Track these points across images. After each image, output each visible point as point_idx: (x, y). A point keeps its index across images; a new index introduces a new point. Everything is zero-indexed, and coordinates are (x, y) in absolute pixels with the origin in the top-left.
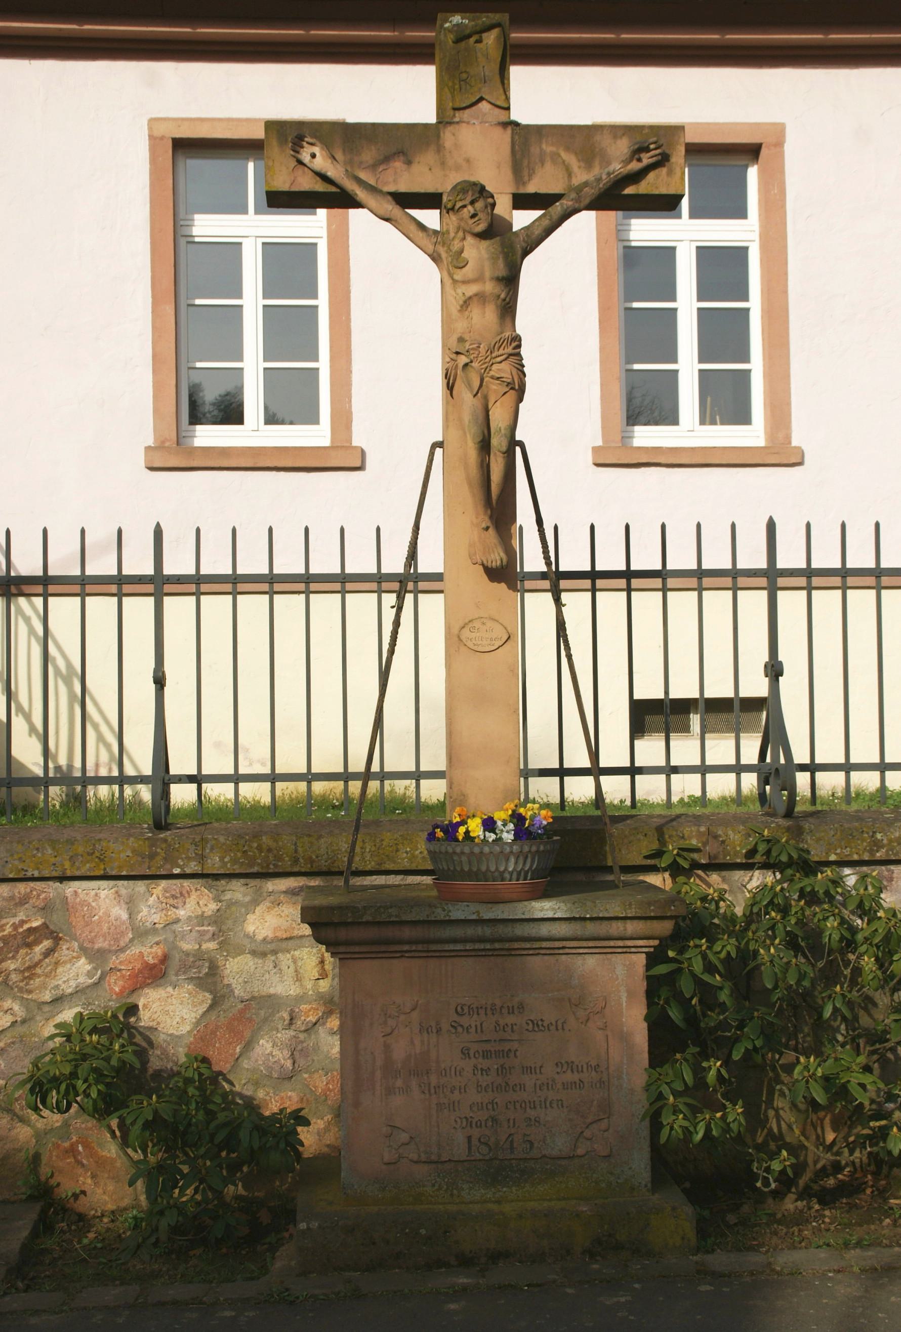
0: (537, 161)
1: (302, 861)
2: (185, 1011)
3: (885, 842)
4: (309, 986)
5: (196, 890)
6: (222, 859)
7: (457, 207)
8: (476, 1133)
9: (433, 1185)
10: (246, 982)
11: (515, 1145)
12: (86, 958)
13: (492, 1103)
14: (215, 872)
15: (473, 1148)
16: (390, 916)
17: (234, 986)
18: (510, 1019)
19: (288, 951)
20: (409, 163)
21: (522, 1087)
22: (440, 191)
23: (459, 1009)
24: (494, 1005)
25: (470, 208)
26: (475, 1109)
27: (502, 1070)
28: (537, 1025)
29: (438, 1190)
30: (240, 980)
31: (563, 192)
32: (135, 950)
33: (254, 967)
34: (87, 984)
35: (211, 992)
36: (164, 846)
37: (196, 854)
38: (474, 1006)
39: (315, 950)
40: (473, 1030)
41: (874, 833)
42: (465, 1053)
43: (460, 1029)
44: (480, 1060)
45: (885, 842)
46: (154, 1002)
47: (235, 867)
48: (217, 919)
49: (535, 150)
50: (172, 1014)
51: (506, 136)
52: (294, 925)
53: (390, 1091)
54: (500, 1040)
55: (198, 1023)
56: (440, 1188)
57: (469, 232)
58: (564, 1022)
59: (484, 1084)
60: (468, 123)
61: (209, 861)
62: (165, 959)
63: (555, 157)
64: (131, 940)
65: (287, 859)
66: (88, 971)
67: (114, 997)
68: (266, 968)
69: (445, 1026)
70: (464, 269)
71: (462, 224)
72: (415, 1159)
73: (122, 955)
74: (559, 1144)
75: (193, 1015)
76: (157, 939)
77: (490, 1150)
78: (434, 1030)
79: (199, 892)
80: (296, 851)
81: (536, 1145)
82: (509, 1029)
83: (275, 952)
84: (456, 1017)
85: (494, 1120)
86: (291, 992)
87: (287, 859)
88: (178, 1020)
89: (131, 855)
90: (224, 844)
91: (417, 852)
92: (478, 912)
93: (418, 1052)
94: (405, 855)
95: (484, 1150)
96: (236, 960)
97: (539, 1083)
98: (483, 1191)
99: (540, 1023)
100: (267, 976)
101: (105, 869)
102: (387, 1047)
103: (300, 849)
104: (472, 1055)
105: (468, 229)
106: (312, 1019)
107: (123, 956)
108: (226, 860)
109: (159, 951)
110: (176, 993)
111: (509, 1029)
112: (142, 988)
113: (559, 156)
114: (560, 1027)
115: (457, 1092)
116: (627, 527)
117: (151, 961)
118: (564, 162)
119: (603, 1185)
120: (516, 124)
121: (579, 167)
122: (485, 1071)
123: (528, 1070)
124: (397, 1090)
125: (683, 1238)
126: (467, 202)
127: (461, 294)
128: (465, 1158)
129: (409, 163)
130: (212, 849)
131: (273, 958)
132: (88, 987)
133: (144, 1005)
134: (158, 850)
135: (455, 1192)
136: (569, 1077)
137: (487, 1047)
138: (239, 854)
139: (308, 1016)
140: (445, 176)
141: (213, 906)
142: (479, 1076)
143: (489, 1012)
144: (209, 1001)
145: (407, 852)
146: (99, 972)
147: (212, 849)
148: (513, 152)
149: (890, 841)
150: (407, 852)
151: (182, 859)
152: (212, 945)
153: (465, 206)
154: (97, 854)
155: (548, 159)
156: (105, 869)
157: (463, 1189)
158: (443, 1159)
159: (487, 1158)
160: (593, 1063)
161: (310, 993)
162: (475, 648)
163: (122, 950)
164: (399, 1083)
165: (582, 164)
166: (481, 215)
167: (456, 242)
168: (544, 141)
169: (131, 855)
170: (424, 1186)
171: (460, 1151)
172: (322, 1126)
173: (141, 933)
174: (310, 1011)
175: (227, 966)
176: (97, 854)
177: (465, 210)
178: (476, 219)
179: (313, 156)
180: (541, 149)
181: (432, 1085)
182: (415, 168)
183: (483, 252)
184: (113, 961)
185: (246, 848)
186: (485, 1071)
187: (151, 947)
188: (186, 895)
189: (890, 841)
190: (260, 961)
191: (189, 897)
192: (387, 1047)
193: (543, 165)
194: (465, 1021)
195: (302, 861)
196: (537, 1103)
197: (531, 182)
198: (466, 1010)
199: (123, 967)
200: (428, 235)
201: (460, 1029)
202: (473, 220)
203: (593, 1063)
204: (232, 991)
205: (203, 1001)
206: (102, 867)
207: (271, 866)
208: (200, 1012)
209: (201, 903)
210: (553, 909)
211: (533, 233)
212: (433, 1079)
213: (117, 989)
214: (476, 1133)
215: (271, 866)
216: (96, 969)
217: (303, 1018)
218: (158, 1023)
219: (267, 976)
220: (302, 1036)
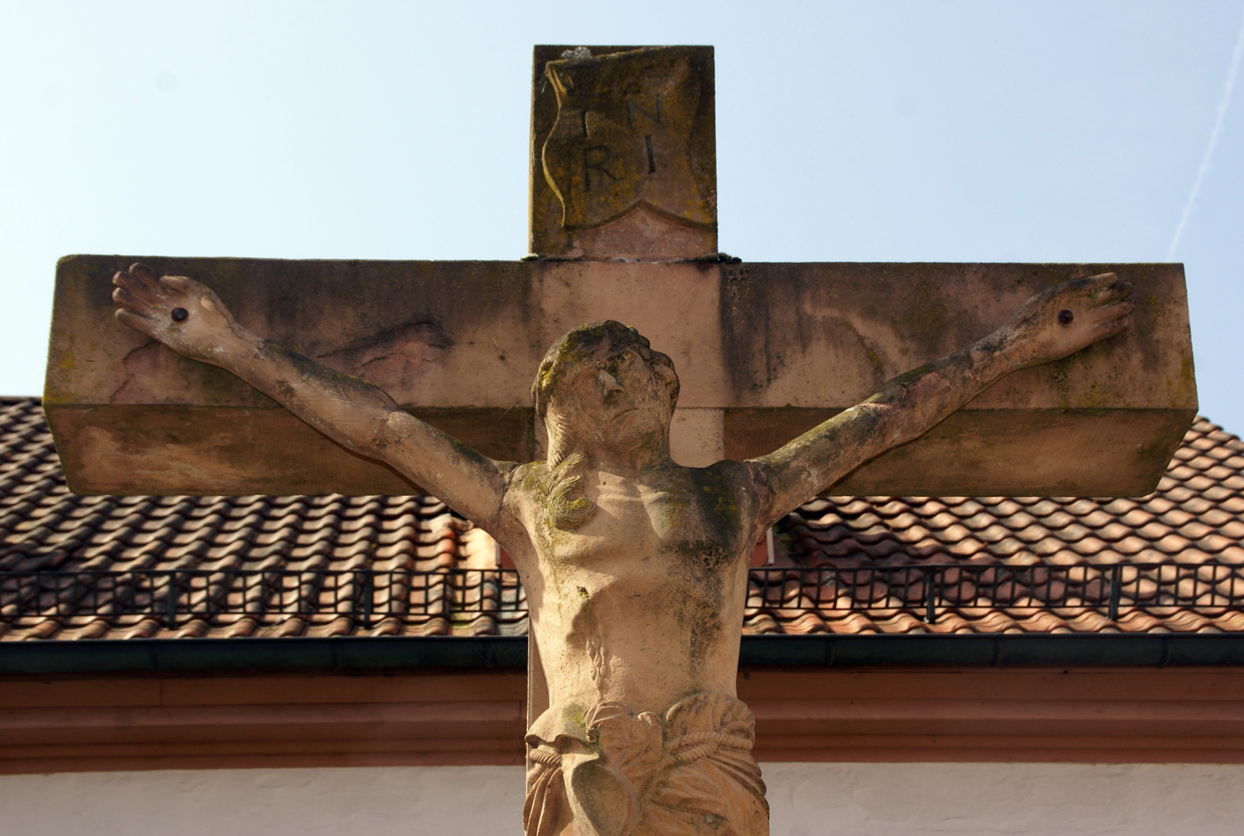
113: (849, 326)
118: (861, 339)
168: (808, 295)
180: (800, 315)
193: (804, 348)
197: (774, 384)
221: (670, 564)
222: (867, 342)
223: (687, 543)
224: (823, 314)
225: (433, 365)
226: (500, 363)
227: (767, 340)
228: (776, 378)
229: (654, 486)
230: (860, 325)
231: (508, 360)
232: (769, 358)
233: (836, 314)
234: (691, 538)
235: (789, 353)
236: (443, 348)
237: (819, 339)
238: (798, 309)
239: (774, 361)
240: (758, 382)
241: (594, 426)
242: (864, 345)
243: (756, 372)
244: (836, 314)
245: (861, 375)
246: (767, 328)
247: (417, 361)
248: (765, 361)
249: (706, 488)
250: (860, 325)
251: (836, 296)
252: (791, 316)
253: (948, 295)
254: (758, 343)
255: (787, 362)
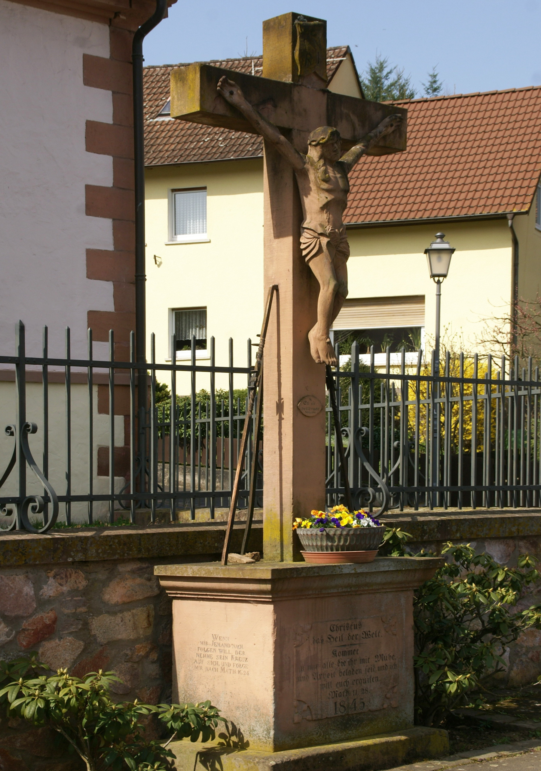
1: (143, 550)
2: (67, 655)
3: (428, 531)
4: (141, 632)
5: (76, 572)
6: (97, 551)
8: (339, 700)
9: (317, 734)
10: (104, 632)
11: (356, 705)
12: (5, 623)
13: (346, 682)
14: (93, 560)
15: (337, 709)
16: (314, 573)
17: (97, 635)
18: (355, 632)
19: (130, 610)
20: (275, 106)
21: (360, 671)
23: (332, 628)
24: (348, 624)
26: (338, 686)
27: (352, 662)
28: (367, 635)
29: (319, 736)
30: (101, 631)
32: (38, 616)
33: (109, 622)
34: (6, 641)
35: (83, 640)
36: (62, 543)
37: (82, 548)
38: (339, 625)
39: (145, 609)
40: (338, 640)
41: (423, 526)
42: (334, 653)
43: (332, 639)
44: (341, 657)
45: (428, 531)
46: (48, 650)
47: (105, 556)
48: (85, 592)
50: (59, 657)
51: (323, 99)
52: (134, 593)
53: (299, 679)
54: (351, 645)
55: (75, 662)
56: (320, 735)
58: (379, 632)
59: (343, 671)
60: (306, 86)
61: (89, 552)
62: (55, 621)
64: (36, 609)
65: (135, 549)
66: (7, 632)
67: (23, 649)
68: (116, 622)
69: (325, 638)
72: (310, 718)
73: (30, 620)
74: (375, 703)
75: (72, 657)
76: (52, 607)
77: (345, 710)
78: (320, 641)
79: (77, 574)
80: (140, 544)
81: (366, 704)
82: (354, 638)
83: (121, 611)
84: (330, 632)
85: (347, 692)
86: (131, 637)
87: (135, 549)
88: (62, 661)
89: (42, 550)
90: (98, 541)
91: (206, 543)
92: (355, 569)
93: (312, 654)
94: (200, 545)
95: (342, 709)
96: (98, 618)
97: (367, 668)
98: (340, 734)
99: (369, 633)
100: (117, 628)
101: (25, 560)
102: (298, 652)
103: (142, 543)
104: (337, 654)
106: (142, 653)
107: (31, 620)
108: (100, 551)
109: (51, 615)
110: (61, 643)
111: (354, 638)
112: (41, 641)
114: (377, 635)
115: (330, 677)
116: (231, 341)
117: (48, 622)
119: (394, 724)
120: (329, 92)
121: (359, 125)
122: (343, 663)
123: (363, 661)
124: (302, 679)
125: (444, 747)
128: (334, 715)
129: (275, 106)
130: (91, 544)
131: (121, 615)
132: (6, 643)
133: (42, 653)
134: (59, 546)
135: (327, 736)
136: (381, 663)
137: (345, 649)
138: (107, 547)
139: (140, 652)
141: (84, 583)
142: (341, 666)
143: (346, 628)
144: (83, 647)
145: (201, 543)
146: (14, 632)
147: (91, 544)
148: (328, 110)
149: (430, 530)
150: (201, 543)
151: (73, 551)
152: (83, 609)
154: (21, 550)
156: (25, 560)
157: (331, 734)
158: (324, 718)
159: (344, 714)
160: (392, 655)
161: (142, 636)
162: (306, 414)
163: (30, 616)
164: (303, 674)
169: (42, 550)
170: (313, 735)
171: (331, 712)
172: (147, 723)
173: (43, 603)
174: (141, 648)
175: (94, 623)
176: (21, 550)
179: (232, 93)
181: (319, 674)
184: (25, 624)
185: (111, 543)
186: (343, 663)
187: (48, 613)
188: (69, 576)
189: (430, 530)
190: (113, 618)
191: (70, 577)
192: (298, 652)
194: (335, 634)
195: (143, 550)
196: (367, 680)
198: (335, 628)
199: (30, 628)
201: (332, 639)
203: (392, 655)
204: (96, 639)
205: (79, 647)
206: (24, 559)
207: (126, 555)
208: (77, 654)
209: (77, 581)
210: (389, 566)
212: (319, 670)
213: (24, 644)
214: (339, 700)
215: (126, 555)
216: (11, 630)
217: (136, 653)
218: (51, 664)
219: (117, 628)
220: (135, 665)
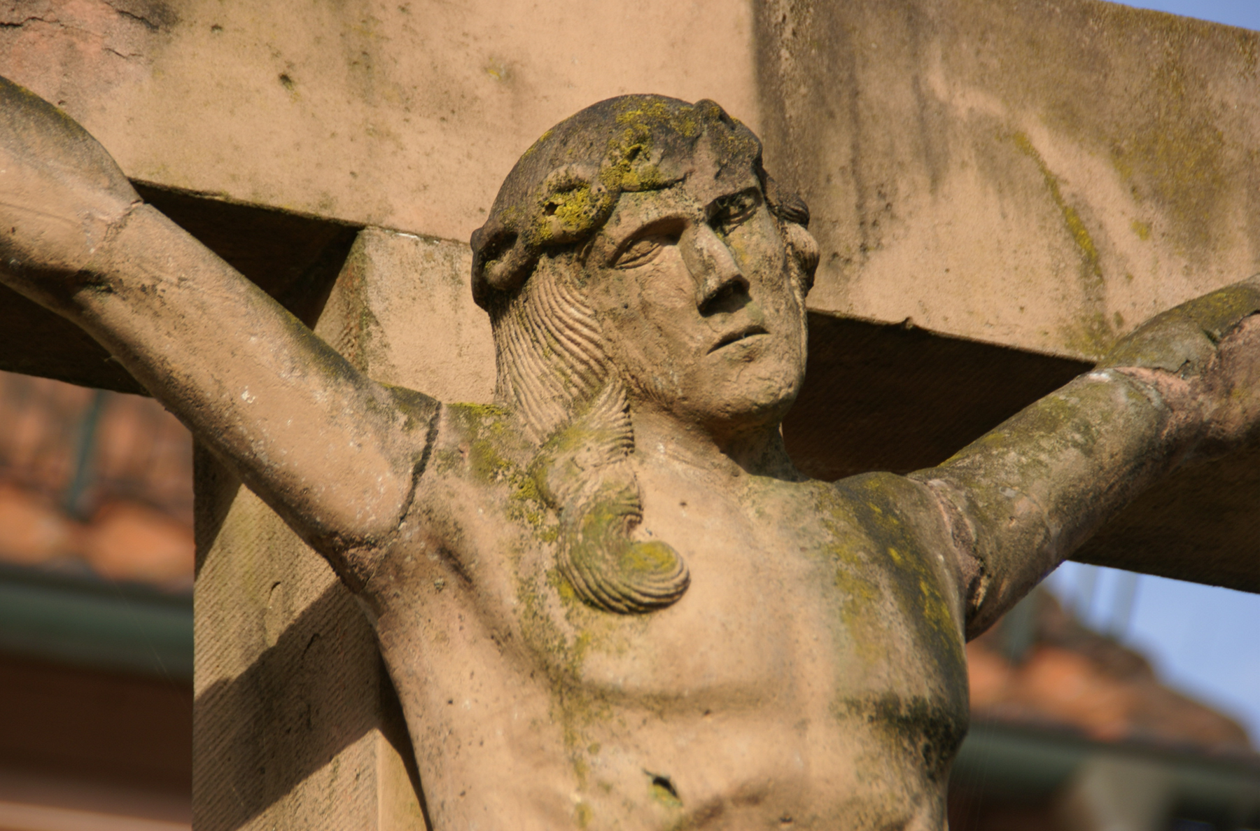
0: (904, 151)
7: (616, 232)
22: (346, 212)
25: (706, 239)
31: (1056, 347)
49: (884, 88)
57: (667, 406)
63: (1001, 154)
70: (661, 619)
71: (631, 349)
105: (665, 379)
113: (1027, 149)
118: (1052, 183)
126: (691, 201)
127: (641, 789)
140: (378, 133)
153: (668, 231)
155: (963, 151)
165: (1159, 219)
166: (761, 305)
167: (589, 452)
168: (935, 49)
177: (669, 255)
178: (740, 319)
180: (923, 100)
182: (192, 53)
183: (767, 536)
193: (935, 181)
197: (877, 261)
200: (371, 405)
202: (722, 325)
211: (1003, 508)
221: (858, 748)
222: (1065, 190)
223: (896, 703)
224: (969, 102)
225: (131, 67)
226: (277, 91)
227: (855, 147)
228: (879, 246)
229: (13, 266)
230: (1043, 141)
231: (301, 89)
232: (862, 192)
233: (994, 107)
234: (905, 691)
235: (903, 187)
236: (153, 28)
237: (964, 165)
238: (916, 80)
239: (873, 204)
240: (841, 249)
241: (662, 354)
242: (1058, 199)
243: (835, 223)
244: (994, 107)
245: (1057, 271)
246: (855, 118)
247: (92, 49)
248: (853, 199)
249: (893, 552)
250: (1043, 141)
251: (995, 63)
252: (903, 98)
253: (1224, 106)
254: (837, 154)
255: (900, 209)
